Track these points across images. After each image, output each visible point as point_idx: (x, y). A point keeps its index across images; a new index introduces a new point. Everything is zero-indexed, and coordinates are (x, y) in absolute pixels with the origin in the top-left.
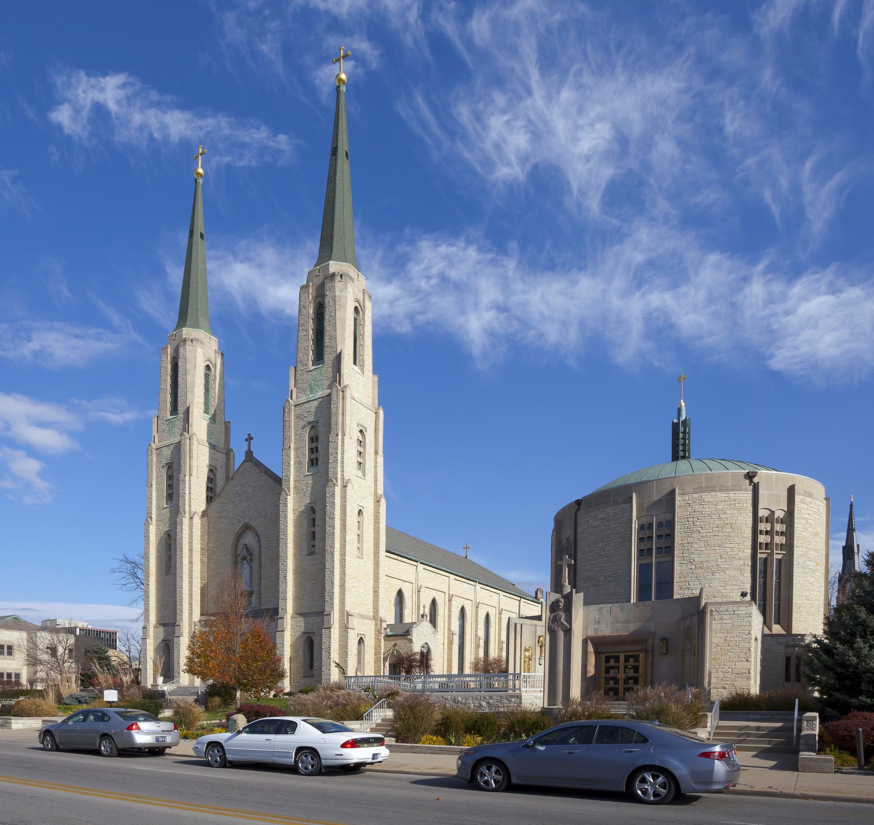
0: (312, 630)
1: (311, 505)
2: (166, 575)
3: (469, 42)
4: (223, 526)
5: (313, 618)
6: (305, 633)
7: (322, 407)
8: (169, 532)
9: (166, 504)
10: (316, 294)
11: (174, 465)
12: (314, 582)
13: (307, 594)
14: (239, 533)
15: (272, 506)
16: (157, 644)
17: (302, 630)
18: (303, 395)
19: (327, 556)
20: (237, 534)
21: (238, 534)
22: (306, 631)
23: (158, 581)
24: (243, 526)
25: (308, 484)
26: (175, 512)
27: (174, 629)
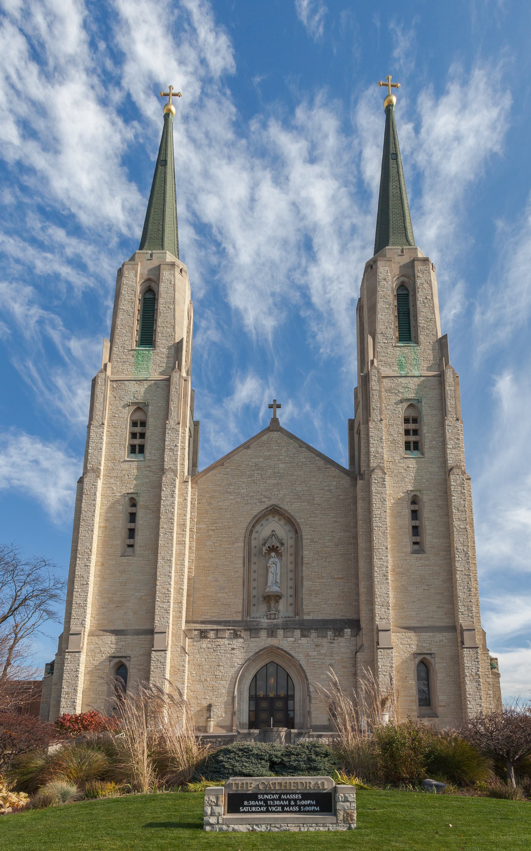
0: (431, 650)
1: (414, 493)
2: (121, 556)
3: (68, 351)
4: (229, 504)
5: (431, 634)
6: (114, 657)
7: (425, 387)
8: (134, 496)
9: (128, 457)
10: (400, 271)
11: (150, 407)
12: (426, 588)
13: (414, 602)
14: (259, 516)
15: (322, 490)
16: (96, 663)
17: (414, 648)
18: (388, 369)
19: (457, 556)
20: (256, 516)
21: (257, 518)
22: (419, 652)
23: (103, 565)
24: (267, 508)
25: (408, 467)
26: (148, 469)
27: (152, 640)
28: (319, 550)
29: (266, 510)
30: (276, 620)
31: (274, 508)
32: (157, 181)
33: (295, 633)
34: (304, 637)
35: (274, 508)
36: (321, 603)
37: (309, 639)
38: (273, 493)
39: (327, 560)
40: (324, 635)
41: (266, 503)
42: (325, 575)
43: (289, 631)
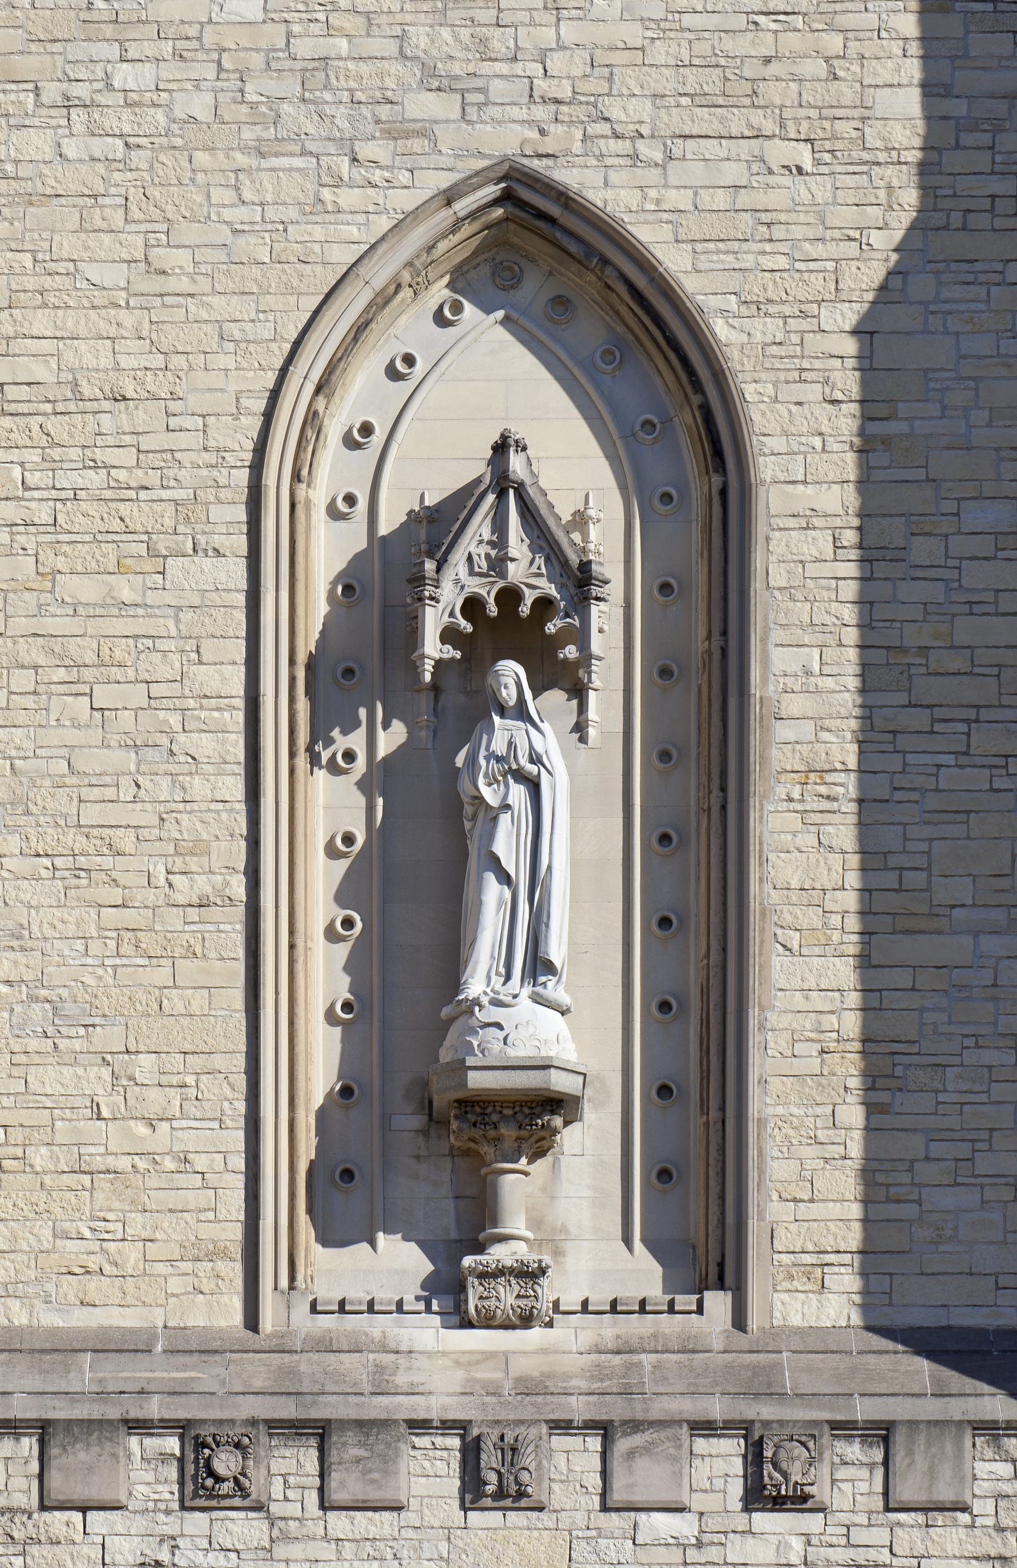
24: (449, 197)
28: (913, 637)
29: (444, 217)
30: (535, 1335)
32: (877, 1391)
33: (701, 1471)
34: (778, 1503)
36: (928, 1172)
37: (813, 1522)
38: (500, 42)
39: (984, 741)
40: (945, 1494)
41: (447, 138)
42: (962, 890)
43: (647, 1449)
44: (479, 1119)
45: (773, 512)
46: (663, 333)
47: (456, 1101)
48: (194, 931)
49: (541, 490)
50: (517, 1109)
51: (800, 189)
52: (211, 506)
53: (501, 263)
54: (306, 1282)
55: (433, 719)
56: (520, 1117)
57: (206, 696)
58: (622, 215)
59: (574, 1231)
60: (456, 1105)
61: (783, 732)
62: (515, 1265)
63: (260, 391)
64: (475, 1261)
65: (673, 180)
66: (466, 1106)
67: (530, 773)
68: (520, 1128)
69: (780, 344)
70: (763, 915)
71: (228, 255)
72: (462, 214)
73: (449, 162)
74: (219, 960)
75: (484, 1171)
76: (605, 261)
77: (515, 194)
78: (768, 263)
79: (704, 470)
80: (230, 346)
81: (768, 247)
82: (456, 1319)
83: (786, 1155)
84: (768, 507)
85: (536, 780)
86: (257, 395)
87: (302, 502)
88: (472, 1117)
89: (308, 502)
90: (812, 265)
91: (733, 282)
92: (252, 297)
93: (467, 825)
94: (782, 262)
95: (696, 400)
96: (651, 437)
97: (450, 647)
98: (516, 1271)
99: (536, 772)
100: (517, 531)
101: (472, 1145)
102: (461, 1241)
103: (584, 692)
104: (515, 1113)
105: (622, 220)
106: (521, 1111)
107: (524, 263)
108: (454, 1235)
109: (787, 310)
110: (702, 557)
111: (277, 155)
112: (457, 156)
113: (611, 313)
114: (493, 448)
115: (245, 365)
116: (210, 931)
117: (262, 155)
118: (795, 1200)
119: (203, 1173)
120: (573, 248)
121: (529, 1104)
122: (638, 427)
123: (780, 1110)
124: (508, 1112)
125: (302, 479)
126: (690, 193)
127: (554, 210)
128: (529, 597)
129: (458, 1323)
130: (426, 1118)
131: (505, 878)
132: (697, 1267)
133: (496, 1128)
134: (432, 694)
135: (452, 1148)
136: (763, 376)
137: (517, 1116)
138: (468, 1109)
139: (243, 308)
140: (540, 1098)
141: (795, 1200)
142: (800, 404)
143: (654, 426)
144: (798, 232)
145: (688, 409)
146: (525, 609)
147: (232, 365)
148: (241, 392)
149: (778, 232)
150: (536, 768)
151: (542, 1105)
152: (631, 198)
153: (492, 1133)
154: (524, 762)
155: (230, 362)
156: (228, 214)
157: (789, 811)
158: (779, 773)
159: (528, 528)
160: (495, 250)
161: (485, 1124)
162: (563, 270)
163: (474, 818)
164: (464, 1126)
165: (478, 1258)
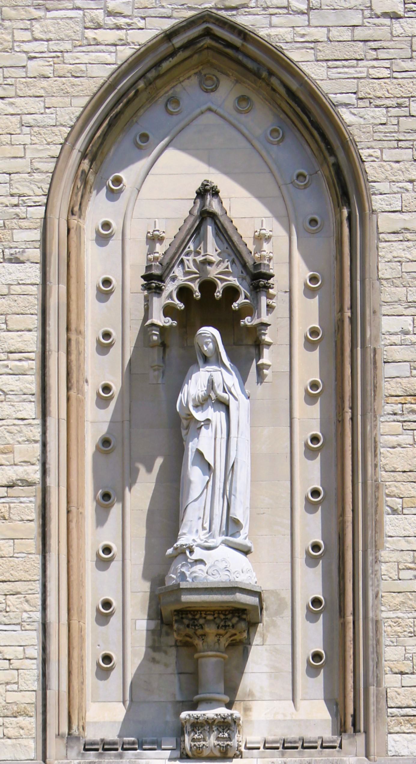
31: (208, 33)
35: (208, 33)
44: (191, 622)
45: (381, 230)
46: (309, 118)
47: (175, 611)
48: (4, 503)
49: (229, 218)
50: (216, 615)
51: (398, 27)
52: (14, 231)
53: (205, 75)
54: (78, 729)
55: (162, 364)
56: (218, 621)
57: (11, 352)
58: (281, 45)
59: (257, 694)
60: (175, 613)
61: (389, 370)
62: (216, 717)
63: (47, 158)
64: (189, 715)
65: (314, 22)
66: (182, 614)
67: (225, 399)
68: (218, 628)
69: (384, 124)
70: (377, 488)
71: (26, 72)
72: (177, 45)
73: (167, 12)
74: (20, 521)
75: (196, 656)
76: (271, 73)
77: (212, 32)
78: (374, 73)
79: (337, 204)
80: (26, 130)
81: (375, 63)
82: (177, 754)
83: (395, 644)
84: (378, 228)
85: (227, 404)
86: (44, 160)
87: (75, 228)
88: (186, 621)
89: (79, 229)
90: (404, 75)
91: (352, 85)
92: (42, 99)
93: (184, 432)
94: (386, 73)
95: (331, 160)
96: (302, 184)
97: (169, 319)
98: (216, 722)
99: (227, 398)
100: (213, 244)
101: (188, 639)
102: (183, 702)
103: (261, 346)
104: (215, 618)
105: (281, 47)
106: (219, 617)
107: (218, 74)
108: (178, 698)
109: (388, 102)
110: (336, 260)
111: (57, 10)
112: (173, 9)
113: (276, 106)
114: (197, 192)
115: (37, 141)
116: (14, 503)
117: (48, 10)
118: (402, 673)
119: (10, 660)
120: (250, 64)
121: (224, 612)
122: (295, 178)
123: (391, 615)
124: (210, 617)
125: (74, 213)
126: (325, 30)
127: (237, 41)
128: (221, 286)
129: (179, 756)
130: (159, 621)
131: (208, 468)
132: (339, 717)
133: (202, 628)
134: (162, 349)
135: (176, 641)
136: (373, 144)
137: (216, 620)
138: (184, 616)
139: (36, 105)
140: (231, 608)
141: (402, 673)
142: (398, 162)
143: (305, 177)
144: (392, 54)
145: (326, 166)
146: (197, 294)
147: (28, 141)
148: (34, 158)
149: (382, 54)
150: (226, 395)
151: (232, 613)
152: (286, 33)
153: (200, 632)
154: (220, 392)
155: (27, 139)
156: (26, 47)
157: (394, 421)
158: (387, 396)
159: (220, 242)
160: (200, 68)
161: (195, 626)
162: (245, 80)
163: (188, 428)
164: (181, 627)
165: (191, 712)
